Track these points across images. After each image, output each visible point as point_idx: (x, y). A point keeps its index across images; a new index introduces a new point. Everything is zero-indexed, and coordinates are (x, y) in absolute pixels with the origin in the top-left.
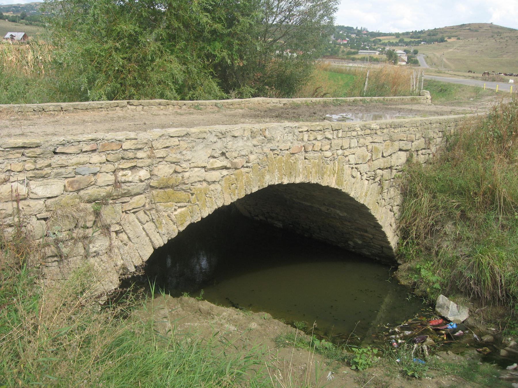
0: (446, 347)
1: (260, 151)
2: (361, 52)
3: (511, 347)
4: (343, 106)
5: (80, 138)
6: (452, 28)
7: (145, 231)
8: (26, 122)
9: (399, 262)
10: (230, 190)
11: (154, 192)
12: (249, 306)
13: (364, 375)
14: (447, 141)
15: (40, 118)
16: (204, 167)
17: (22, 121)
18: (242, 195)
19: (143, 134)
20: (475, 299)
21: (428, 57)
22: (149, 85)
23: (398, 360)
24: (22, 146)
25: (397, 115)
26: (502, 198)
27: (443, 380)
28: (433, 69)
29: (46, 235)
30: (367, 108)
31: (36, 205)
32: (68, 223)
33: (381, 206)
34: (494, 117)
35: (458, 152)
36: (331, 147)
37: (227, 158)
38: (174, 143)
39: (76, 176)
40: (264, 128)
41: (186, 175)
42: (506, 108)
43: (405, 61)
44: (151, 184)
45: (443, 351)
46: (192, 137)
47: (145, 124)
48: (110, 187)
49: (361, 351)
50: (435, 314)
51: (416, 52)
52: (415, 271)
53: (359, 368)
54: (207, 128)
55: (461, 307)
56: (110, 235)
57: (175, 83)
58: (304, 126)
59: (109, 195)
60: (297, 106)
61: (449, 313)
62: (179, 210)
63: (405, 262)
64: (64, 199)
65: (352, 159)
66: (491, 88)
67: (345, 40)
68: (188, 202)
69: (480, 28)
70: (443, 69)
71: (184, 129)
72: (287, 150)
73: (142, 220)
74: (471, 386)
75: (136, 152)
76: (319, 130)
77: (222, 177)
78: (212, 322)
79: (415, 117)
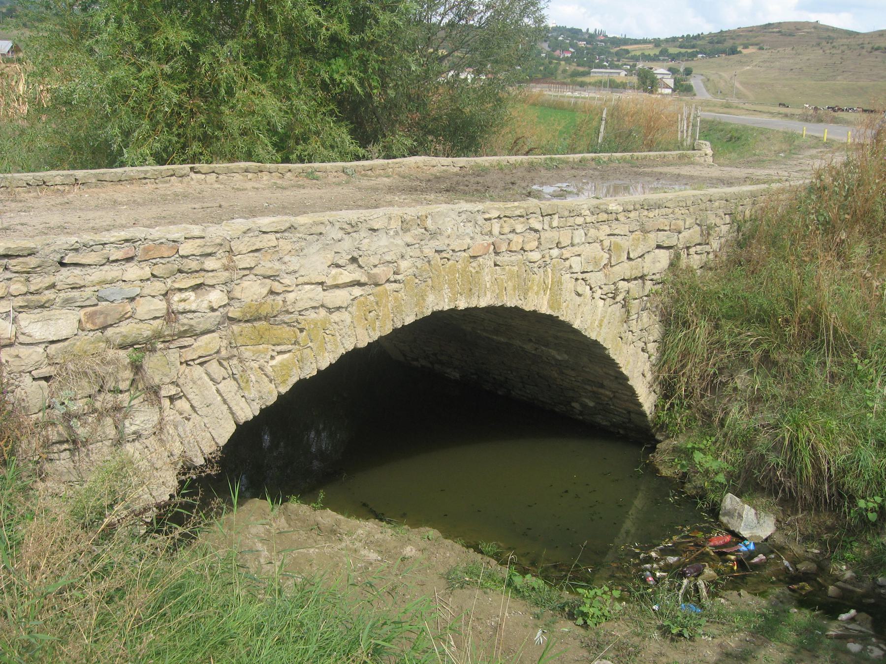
0: (736, 583)
1: (418, 254)
2: (595, 72)
3: (845, 582)
4: (563, 169)
5: (106, 237)
6: (751, 30)
7: (220, 394)
8: (13, 205)
9: (659, 437)
10: (366, 322)
11: (236, 328)
12: (402, 517)
13: (597, 634)
14: (739, 230)
15: (38, 198)
16: (322, 283)
17: (7, 203)
18: (388, 330)
19: (215, 228)
20: (786, 501)
21: (708, 80)
22: (226, 137)
23: (655, 607)
24: (4, 253)
25: (655, 184)
26: (831, 328)
27: (731, 641)
28: (719, 100)
29: (49, 406)
30: (603, 173)
31: (30, 355)
32: (86, 384)
33: (626, 344)
34: (817, 190)
35: (758, 250)
36: (540, 244)
37: (360, 266)
38: (269, 243)
39: (99, 303)
40: (424, 214)
41: (291, 297)
42: (838, 173)
43: (670, 88)
44: (230, 315)
45: (731, 589)
46: (299, 233)
47: (220, 206)
48: (158, 321)
49: (592, 593)
50: (719, 526)
51: (688, 72)
52: (684, 453)
53: (589, 622)
54: (326, 216)
55: (763, 514)
56: (160, 403)
57: (272, 130)
58: (494, 208)
59: (158, 336)
60: (482, 172)
61: (742, 525)
62: (279, 358)
63: (668, 437)
64: (78, 343)
65: (576, 264)
66: (817, 135)
67: (568, 51)
68: (295, 344)
69: (798, 29)
70: (734, 101)
71: (286, 218)
72: (464, 250)
73: (215, 376)
74: (777, 650)
75: (203, 259)
76: (520, 216)
77: (353, 300)
78: (339, 547)
79: (685, 190)
